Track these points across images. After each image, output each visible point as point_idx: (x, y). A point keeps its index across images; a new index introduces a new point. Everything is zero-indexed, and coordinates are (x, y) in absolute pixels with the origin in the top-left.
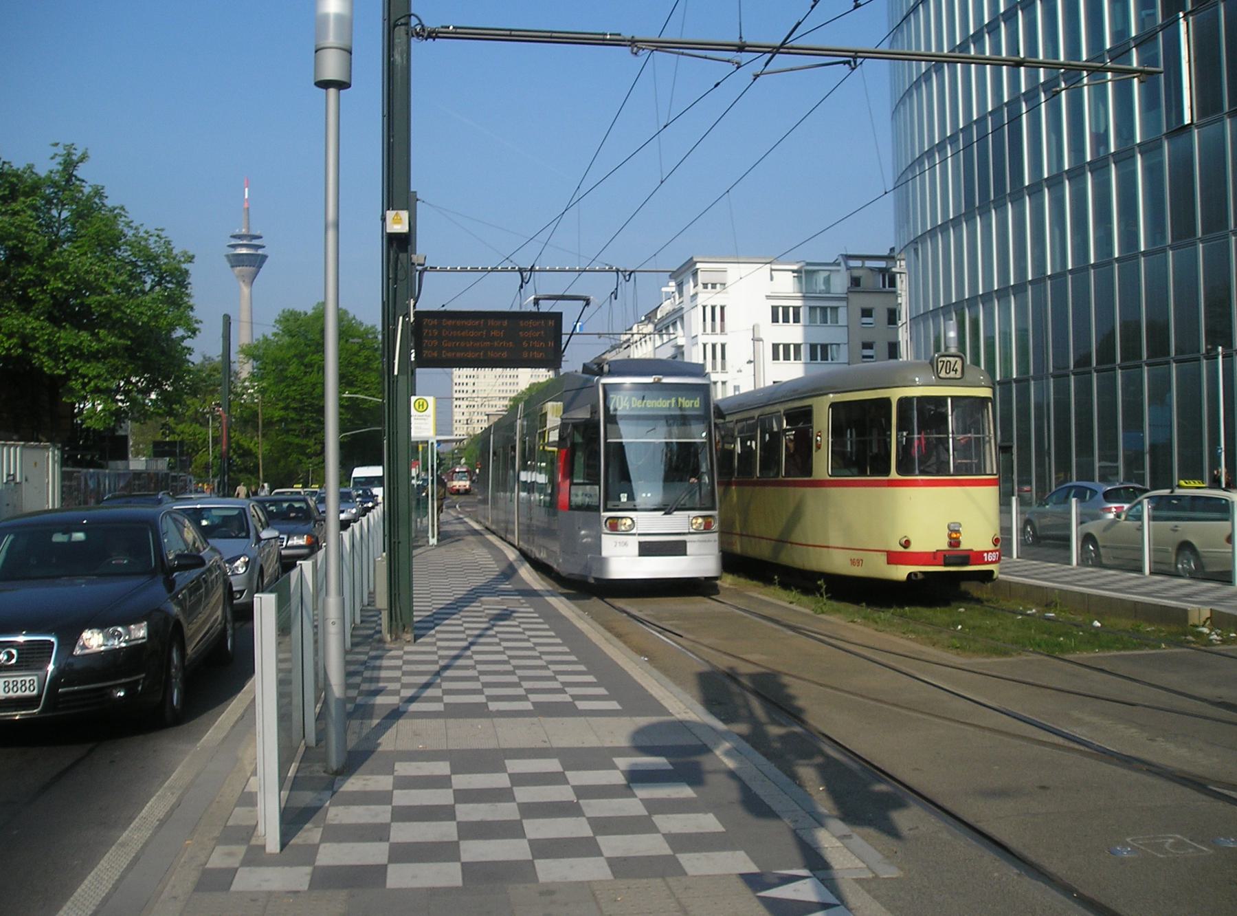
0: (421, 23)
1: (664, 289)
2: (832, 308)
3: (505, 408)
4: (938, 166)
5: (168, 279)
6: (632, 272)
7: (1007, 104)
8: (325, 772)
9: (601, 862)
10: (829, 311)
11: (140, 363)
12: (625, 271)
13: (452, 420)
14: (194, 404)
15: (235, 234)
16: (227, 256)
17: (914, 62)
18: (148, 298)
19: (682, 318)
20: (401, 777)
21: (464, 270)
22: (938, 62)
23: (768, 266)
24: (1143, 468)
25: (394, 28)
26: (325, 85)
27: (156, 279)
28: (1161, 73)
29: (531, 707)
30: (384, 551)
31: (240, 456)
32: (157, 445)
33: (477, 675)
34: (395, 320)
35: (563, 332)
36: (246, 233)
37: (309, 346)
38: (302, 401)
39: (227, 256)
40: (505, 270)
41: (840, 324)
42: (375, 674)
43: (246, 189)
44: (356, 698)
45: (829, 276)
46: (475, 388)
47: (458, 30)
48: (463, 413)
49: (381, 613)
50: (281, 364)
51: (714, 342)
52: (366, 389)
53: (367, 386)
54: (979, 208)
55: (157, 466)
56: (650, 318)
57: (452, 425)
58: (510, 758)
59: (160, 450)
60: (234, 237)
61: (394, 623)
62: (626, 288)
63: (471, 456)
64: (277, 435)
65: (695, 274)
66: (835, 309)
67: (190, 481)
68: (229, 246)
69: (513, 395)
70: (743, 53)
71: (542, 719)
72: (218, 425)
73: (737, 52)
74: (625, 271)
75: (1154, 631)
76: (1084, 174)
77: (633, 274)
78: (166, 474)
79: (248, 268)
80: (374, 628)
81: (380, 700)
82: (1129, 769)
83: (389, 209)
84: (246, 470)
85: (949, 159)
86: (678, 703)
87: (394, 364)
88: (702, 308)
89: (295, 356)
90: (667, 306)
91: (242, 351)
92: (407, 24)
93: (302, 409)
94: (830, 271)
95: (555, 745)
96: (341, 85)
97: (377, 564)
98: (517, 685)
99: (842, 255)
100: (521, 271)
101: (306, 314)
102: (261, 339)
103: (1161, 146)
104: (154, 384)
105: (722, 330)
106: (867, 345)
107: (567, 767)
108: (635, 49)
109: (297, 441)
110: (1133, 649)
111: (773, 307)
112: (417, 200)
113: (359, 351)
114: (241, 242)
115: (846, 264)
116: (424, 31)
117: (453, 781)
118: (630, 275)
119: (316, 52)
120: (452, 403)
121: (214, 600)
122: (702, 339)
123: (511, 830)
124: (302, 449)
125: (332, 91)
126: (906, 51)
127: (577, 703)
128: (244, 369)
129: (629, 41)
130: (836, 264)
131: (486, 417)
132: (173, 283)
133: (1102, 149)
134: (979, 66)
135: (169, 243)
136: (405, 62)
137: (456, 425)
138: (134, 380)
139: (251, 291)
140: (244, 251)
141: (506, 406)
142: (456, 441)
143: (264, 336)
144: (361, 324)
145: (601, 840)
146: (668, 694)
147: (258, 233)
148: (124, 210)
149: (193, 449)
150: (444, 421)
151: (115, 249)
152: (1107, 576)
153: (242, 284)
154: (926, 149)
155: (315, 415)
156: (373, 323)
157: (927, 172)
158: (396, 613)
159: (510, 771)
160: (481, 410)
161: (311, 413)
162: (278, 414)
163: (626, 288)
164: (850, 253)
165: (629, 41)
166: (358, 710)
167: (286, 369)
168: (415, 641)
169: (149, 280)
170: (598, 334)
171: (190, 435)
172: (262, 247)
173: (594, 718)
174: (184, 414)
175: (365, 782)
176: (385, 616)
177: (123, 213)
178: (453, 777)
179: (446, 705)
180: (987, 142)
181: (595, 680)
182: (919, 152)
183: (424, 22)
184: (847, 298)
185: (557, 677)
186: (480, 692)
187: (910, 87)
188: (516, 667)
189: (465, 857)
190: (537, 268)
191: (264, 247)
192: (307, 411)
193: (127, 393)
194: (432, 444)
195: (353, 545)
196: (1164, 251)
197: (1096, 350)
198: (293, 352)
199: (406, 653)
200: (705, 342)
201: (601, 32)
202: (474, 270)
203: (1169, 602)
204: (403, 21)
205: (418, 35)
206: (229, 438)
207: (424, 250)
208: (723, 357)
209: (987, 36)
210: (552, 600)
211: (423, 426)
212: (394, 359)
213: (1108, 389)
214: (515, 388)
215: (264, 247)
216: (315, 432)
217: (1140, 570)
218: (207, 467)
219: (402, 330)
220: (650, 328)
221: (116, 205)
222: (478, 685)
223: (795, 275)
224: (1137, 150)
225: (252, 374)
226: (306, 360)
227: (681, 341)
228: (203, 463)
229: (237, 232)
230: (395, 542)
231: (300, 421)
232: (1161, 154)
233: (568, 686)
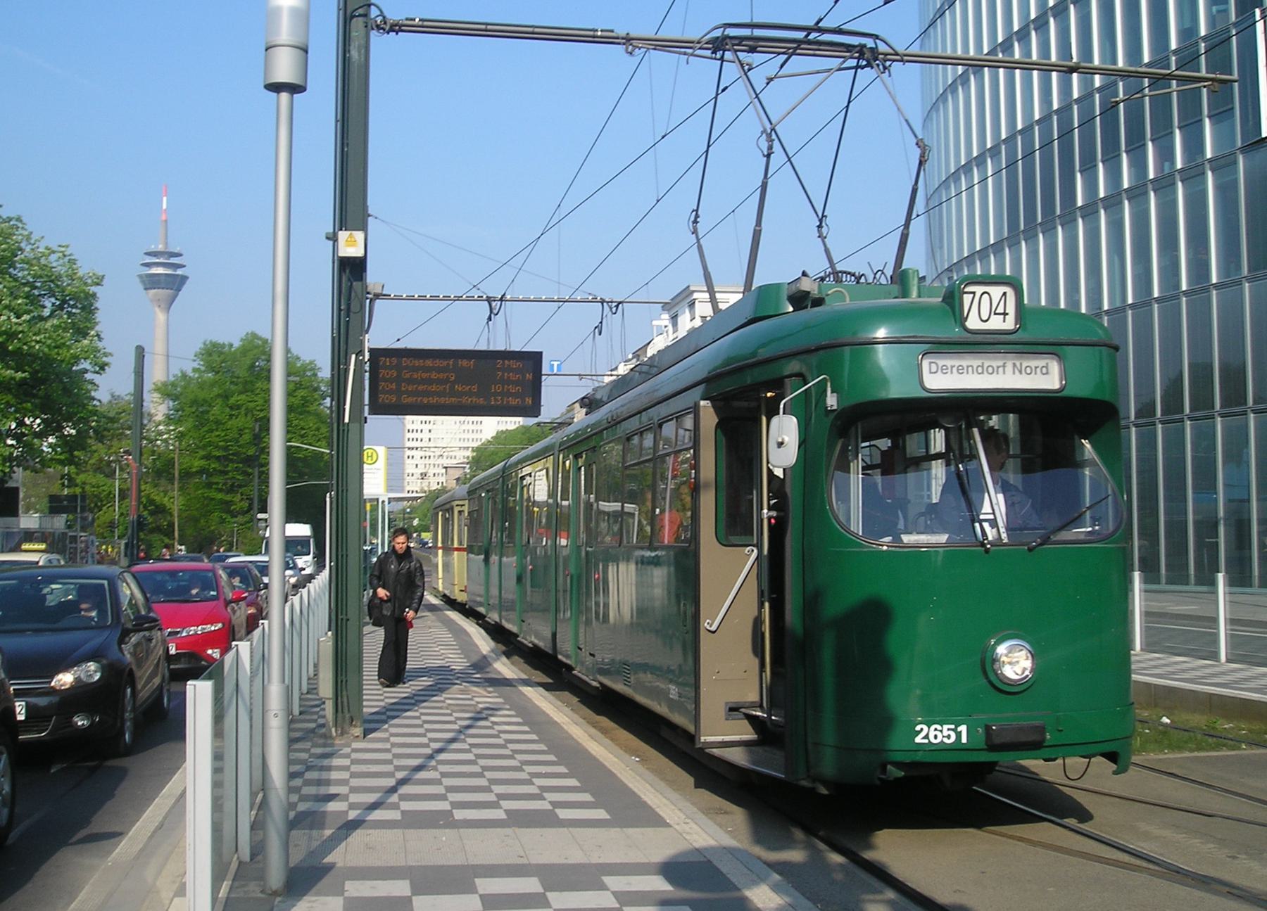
0: (382, 14)
1: (655, 323)
3: (466, 460)
4: (976, 187)
5: (71, 303)
6: (620, 303)
7: (1056, 111)
8: (262, 892)
11: (37, 401)
12: (612, 302)
13: (403, 474)
14: (100, 451)
15: (149, 251)
16: (140, 276)
17: (949, 66)
18: (48, 325)
20: (353, 898)
21: (422, 298)
22: (976, 65)
24: (1217, 536)
25: (351, 20)
26: (276, 88)
27: (58, 303)
28: (1236, 81)
29: (504, 816)
30: (330, 630)
31: (152, 513)
32: (54, 499)
33: (439, 777)
34: (346, 359)
35: (543, 373)
36: (162, 250)
37: (236, 385)
38: (226, 448)
39: (140, 276)
40: (470, 299)
42: (324, 775)
43: (165, 199)
46: (432, 436)
47: (426, 23)
48: (417, 465)
49: (324, 703)
50: (202, 405)
52: (302, 436)
53: (303, 432)
54: (1060, 217)
55: (52, 524)
56: (638, 356)
57: (404, 479)
58: (480, 877)
59: (56, 505)
61: (340, 714)
62: (613, 322)
63: (425, 516)
64: (197, 489)
65: (692, 305)
67: (92, 541)
68: (142, 265)
69: (476, 445)
70: (755, 54)
71: (517, 830)
72: (125, 476)
73: (748, 52)
74: (612, 302)
75: (1232, 728)
76: (1146, 193)
77: (620, 305)
78: (63, 533)
79: (165, 291)
80: (315, 721)
81: (332, 806)
82: (1207, 891)
83: (341, 230)
84: (158, 529)
85: (990, 180)
86: (678, 812)
87: (344, 409)
89: (219, 396)
91: (157, 390)
92: (365, 15)
93: (226, 458)
95: (533, 862)
96: (295, 89)
97: (321, 644)
98: (487, 790)
100: (489, 300)
101: (231, 345)
103: (1235, 162)
104: (52, 427)
107: (549, 887)
108: (630, 47)
109: (220, 496)
110: (1207, 751)
112: (369, 216)
113: (295, 391)
114: (158, 261)
116: (385, 23)
117: (414, 903)
118: (617, 307)
119: (266, 50)
124: (226, 506)
125: (284, 96)
126: (940, 53)
127: (557, 811)
128: (158, 409)
129: (623, 38)
131: (444, 470)
132: (77, 307)
133: (1167, 164)
134: (1025, 71)
135: (72, 262)
136: (363, 59)
137: (408, 479)
138: (27, 421)
139: (168, 319)
140: (160, 270)
141: (468, 457)
142: (408, 499)
143: (182, 372)
144: (298, 358)
146: (664, 800)
147: (177, 250)
148: (21, 221)
149: (96, 505)
150: (395, 476)
151: (10, 267)
152: (1176, 663)
153: (157, 310)
154: (963, 163)
155: (241, 465)
156: (312, 358)
158: (342, 702)
159: (481, 892)
160: (440, 461)
161: (238, 463)
162: (197, 464)
163: (613, 322)
165: (623, 38)
166: (301, 821)
167: (208, 412)
168: (364, 737)
169: (48, 303)
170: (579, 375)
171: (93, 487)
173: (578, 829)
174: (86, 462)
175: (310, 905)
176: (329, 707)
177: (20, 225)
178: (414, 898)
179: (403, 812)
180: (1034, 160)
181: (578, 784)
182: (955, 166)
183: (386, 14)
185: (534, 780)
186: (442, 797)
187: (945, 91)
188: (485, 768)
190: (508, 297)
191: (184, 266)
192: (232, 461)
193: (18, 437)
194: (383, 502)
195: (292, 622)
196: (1239, 283)
197: (1161, 397)
198: (216, 391)
199: (355, 750)
201: (591, 27)
202: (435, 298)
204: (361, 11)
205: (379, 28)
206: (140, 491)
207: (374, 277)
209: (1033, 33)
210: (527, 690)
211: (374, 483)
212: (345, 404)
213: (1175, 444)
214: (478, 436)
215: (184, 266)
216: (240, 486)
217: (1214, 656)
218: (112, 525)
219: (355, 370)
221: (12, 216)
222: (439, 790)
224: (1207, 166)
225: (168, 417)
226: (232, 401)
228: (108, 521)
229: (153, 248)
230: (342, 619)
231: (226, 473)
232: (1236, 172)
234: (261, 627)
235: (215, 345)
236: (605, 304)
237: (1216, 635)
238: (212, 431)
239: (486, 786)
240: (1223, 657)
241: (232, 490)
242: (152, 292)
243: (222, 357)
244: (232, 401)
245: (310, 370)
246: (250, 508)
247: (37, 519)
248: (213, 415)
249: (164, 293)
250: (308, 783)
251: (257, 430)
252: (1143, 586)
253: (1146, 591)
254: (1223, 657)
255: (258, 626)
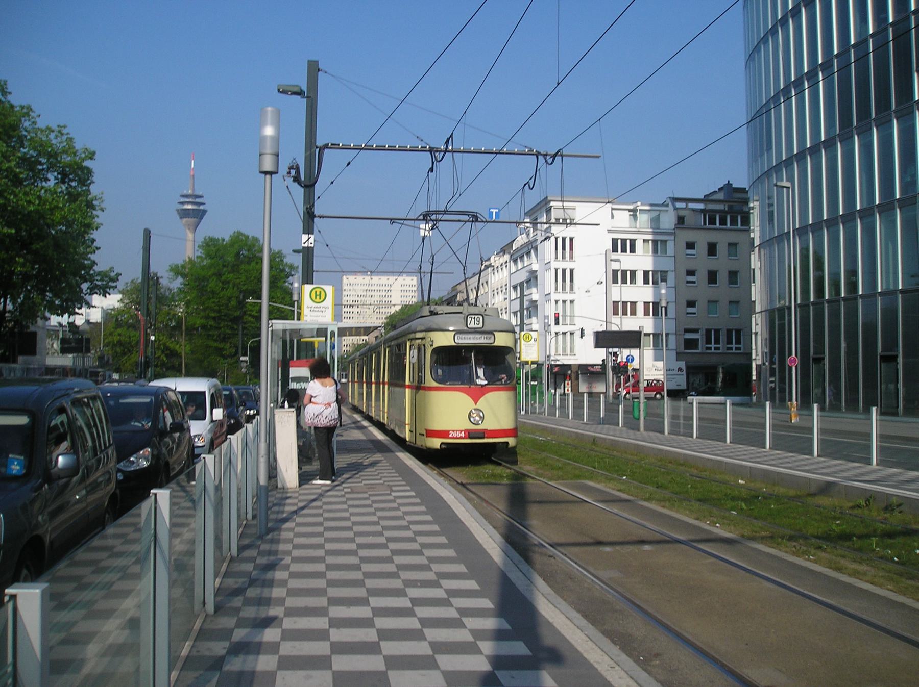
2: (662, 241)
4: (807, 91)
9: (400, 581)
10: (659, 243)
15: (183, 194)
16: (178, 210)
19: (536, 249)
23: (609, 205)
31: (167, 356)
36: (191, 193)
38: (219, 311)
39: (178, 210)
40: (414, 150)
41: (668, 254)
43: (193, 162)
44: (232, 631)
45: (659, 215)
51: (564, 267)
54: (895, 112)
60: (183, 196)
65: (549, 211)
66: (664, 242)
88: (554, 239)
89: (214, 274)
90: (521, 240)
93: (219, 318)
94: (660, 211)
99: (670, 198)
100: (431, 150)
101: (223, 240)
102: (188, 260)
105: (571, 257)
106: (691, 273)
109: (215, 344)
111: (613, 239)
112: (319, 70)
115: (674, 205)
120: (341, 310)
121: (185, 443)
122: (554, 265)
123: (371, 648)
130: (664, 205)
140: (190, 207)
145: (426, 631)
147: (200, 193)
153: (188, 231)
157: (782, 104)
162: (199, 322)
164: (676, 196)
172: (203, 204)
184: (675, 233)
189: (335, 667)
198: (213, 271)
200: (556, 267)
203: (912, 493)
208: (572, 280)
216: (229, 338)
217: (811, 453)
220: (507, 257)
223: (631, 213)
226: (223, 278)
227: (535, 267)
229: (185, 192)
231: (219, 328)
233: (455, 596)
234: (256, 419)
235: (212, 239)
236: (540, 157)
237: (812, 439)
238: (210, 299)
239: (437, 654)
240: (728, 441)
241: (224, 339)
242: (185, 220)
243: (217, 248)
244: (223, 278)
245: (278, 257)
246: (236, 353)
247: (72, 359)
248: (210, 287)
249: (192, 220)
250: (248, 602)
251: (241, 297)
252: (819, 413)
253: (799, 415)
254: (728, 441)
255: (200, 460)
